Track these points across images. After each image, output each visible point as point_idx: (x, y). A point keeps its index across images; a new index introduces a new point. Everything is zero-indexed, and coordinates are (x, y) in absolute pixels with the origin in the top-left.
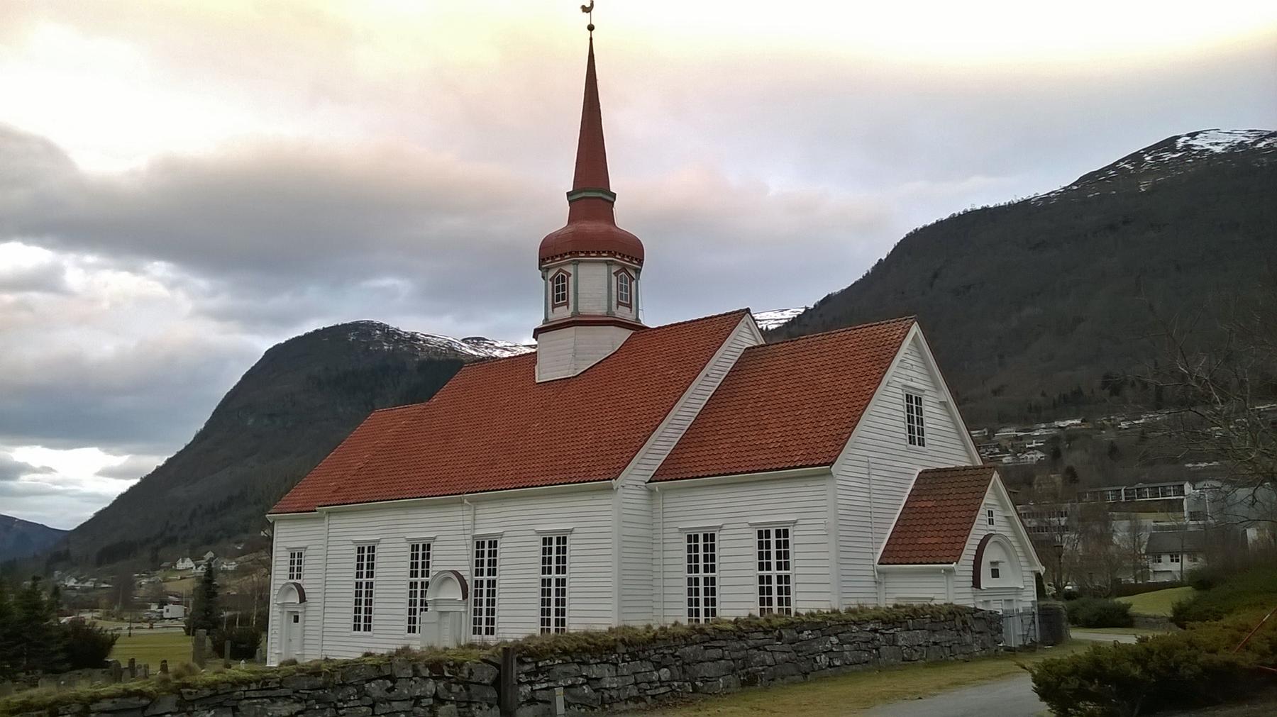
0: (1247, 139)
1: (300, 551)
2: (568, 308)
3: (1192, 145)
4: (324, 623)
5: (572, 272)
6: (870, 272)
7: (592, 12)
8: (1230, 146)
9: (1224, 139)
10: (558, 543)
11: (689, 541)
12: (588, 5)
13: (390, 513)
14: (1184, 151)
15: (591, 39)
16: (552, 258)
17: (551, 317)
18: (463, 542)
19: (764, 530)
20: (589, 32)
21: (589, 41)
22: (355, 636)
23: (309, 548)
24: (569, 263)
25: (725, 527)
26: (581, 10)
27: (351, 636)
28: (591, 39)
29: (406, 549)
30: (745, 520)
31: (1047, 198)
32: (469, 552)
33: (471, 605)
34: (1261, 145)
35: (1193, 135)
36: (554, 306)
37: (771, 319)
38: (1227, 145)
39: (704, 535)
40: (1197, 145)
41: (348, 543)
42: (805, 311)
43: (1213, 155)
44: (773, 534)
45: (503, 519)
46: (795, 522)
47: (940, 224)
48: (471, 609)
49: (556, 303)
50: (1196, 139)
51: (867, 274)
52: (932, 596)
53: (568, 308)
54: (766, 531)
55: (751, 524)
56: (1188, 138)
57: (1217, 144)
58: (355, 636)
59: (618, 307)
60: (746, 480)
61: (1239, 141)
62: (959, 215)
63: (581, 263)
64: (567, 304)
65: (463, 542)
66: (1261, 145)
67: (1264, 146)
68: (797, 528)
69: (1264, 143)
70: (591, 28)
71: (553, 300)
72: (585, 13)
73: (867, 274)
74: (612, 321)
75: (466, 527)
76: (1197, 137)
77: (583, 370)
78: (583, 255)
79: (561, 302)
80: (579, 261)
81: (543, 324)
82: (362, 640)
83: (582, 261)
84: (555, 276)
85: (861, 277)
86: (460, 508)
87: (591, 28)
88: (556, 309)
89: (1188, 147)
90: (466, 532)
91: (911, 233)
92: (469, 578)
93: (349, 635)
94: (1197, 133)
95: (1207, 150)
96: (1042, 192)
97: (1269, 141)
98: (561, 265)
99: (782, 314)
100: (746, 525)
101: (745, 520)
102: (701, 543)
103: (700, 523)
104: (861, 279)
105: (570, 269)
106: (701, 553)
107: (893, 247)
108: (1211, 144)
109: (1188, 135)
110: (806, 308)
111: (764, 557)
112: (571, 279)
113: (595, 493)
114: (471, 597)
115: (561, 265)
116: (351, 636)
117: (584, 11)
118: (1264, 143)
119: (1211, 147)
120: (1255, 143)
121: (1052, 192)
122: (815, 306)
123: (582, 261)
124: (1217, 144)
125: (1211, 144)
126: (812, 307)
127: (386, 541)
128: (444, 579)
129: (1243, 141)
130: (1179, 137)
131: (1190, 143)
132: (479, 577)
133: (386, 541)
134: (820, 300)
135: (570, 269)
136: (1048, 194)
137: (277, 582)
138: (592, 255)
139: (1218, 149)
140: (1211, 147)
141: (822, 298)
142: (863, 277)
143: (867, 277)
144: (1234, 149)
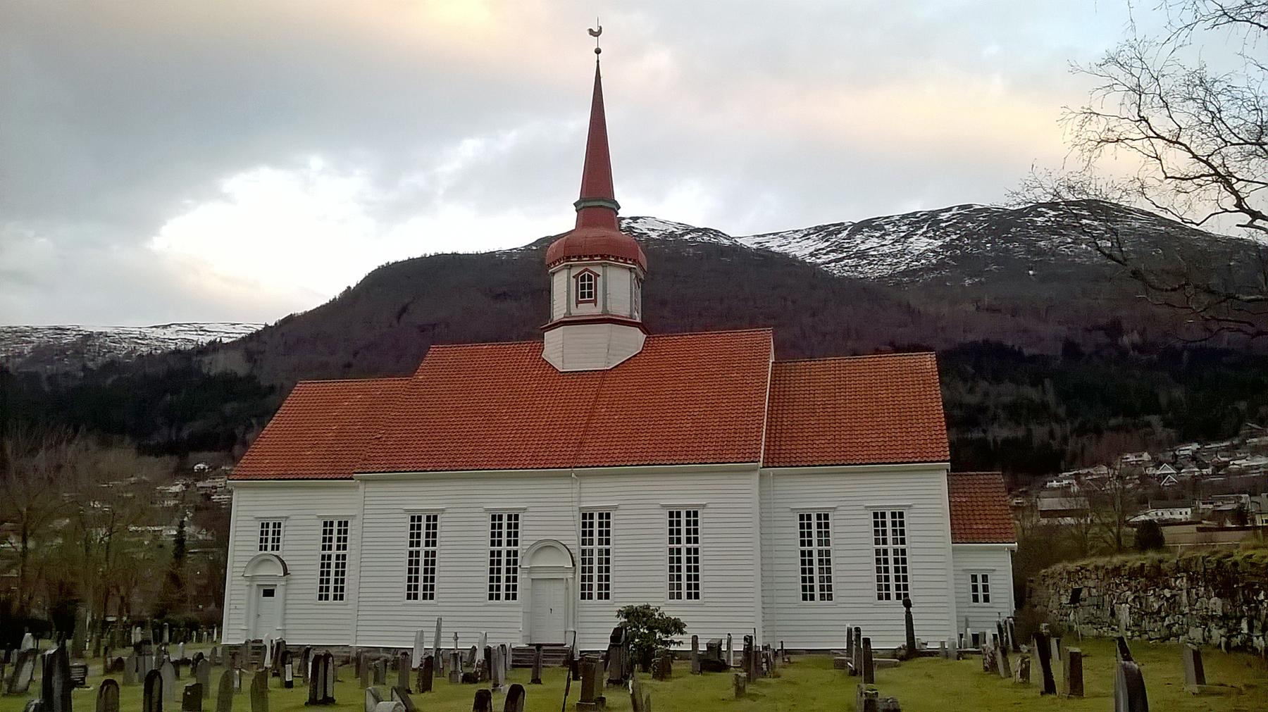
0: (676, 230)
1: (435, 513)
2: (595, 305)
3: (633, 227)
4: (360, 588)
5: (601, 274)
6: (337, 297)
7: (599, 37)
8: (663, 234)
9: (659, 227)
10: (274, 527)
11: (263, 527)
12: (596, 30)
13: (455, 483)
14: (627, 231)
15: (598, 61)
16: (591, 256)
17: (575, 311)
18: (571, 514)
19: (277, 522)
20: (596, 55)
21: (596, 64)
22: (407, 605)
23: (292, 517)
24: (597, 264)
25: (292, 517)
26: (588, 33)
27: (404, 605)
28: (598, 61)
29: (405, 520)
30: (401, 506)
31: (510, 253)
32: (577, 524)
33: (579, 573)
34: (687, 237)
35: (635, 219)
36: (578, 303)
37: (222, 332)
38: (661, 232)
39: (600, 514)
40: (637, 229)
41: (312, 517)
42: (264, 328)
43: (649, 239)
44: (336, 524)
45: (376, 498)
46: (287, 518)
47: (412, 261)
48: (579, 576)
49: (580, 299)
50: (637, 223)
51: (334, 299)
52: (994, 568)
53: (595, 305)
54: (606, 513)
55: (866, 507)
56: (631, 221)
57: (653, 230)
58: (407, 605)
59: (577, 306)
60: (883, 470)
61: (671, 231)
62: (431, 256)
63: (573, 268)
64: (595, 302)
65: (571, 514)
66: (687, 237)
67: (690, 238)
68: (911, 511)
69: (689, 236)
70: (598, 51)
71: (577, 297)
72: (592, 36)
73: (335, 299)
74: (609, 319)
75: (574, 499)
76: (638, 221)
77: (615, 365)
78: (613, 259)
79: (587, 299)
80: (571, 266)
81: (564, 317)
82: (420, 608)
83: (610, 265)
84: (580, 274)
85: (328, 302)
86: (569, 481)
87: (598, 51)
88: (579, 305)
89: (630, 229)
90: (574, 504)
91: (383, 266)
92: (576, 548)
93: (400, 603)
94: (638, 218)
95: (645, 234)
96: (506, 246)
97: (694, 235)
98: (588, 265)
99: (234, 328)
100: (788, 510)
101: (401, 506)
102: (271, 529)
103: (814, 504)
104: (327, 304)
105: (598, 270)
106: (423, 531)
107: (364, 277)
108: (648, 229)
109: (631, 218)
110: (266, 325)
111: (674, 533)
112: (600, 280)
113: (731, 473)
114: (579, 565)
115: (588, 265)
116: (404, 605)
117: (591, 34)
118: (689, 236)
119: (648, 232)
120: (682, 235)
121: (514, 249)
122: (276, 324)
123: (610, 265)
124: (653, 230)
125: (648, 229)
126: (273, 324)
127: (450, 511)
128: (545, 546)
129: (673, 232)
130: (624, 219)
131: (632, 225)
132: (512, 547)
133: (450, 511)
134: (281, 319)
135: (598, 270)
136: (510, 250)
137: (525, 543)
138: (595, 258)
139: (654, 235)
140: (648, 232)
141: (283, 317)
142: (330, 301)
143: (333, 303)
144: (666, 237)
